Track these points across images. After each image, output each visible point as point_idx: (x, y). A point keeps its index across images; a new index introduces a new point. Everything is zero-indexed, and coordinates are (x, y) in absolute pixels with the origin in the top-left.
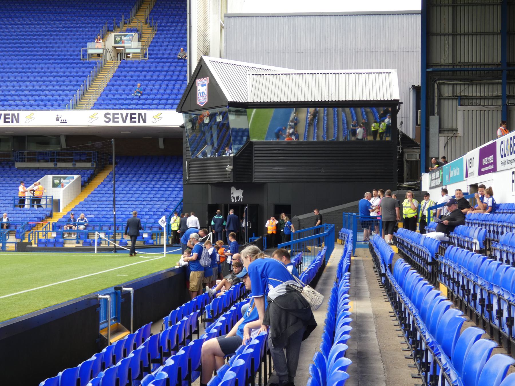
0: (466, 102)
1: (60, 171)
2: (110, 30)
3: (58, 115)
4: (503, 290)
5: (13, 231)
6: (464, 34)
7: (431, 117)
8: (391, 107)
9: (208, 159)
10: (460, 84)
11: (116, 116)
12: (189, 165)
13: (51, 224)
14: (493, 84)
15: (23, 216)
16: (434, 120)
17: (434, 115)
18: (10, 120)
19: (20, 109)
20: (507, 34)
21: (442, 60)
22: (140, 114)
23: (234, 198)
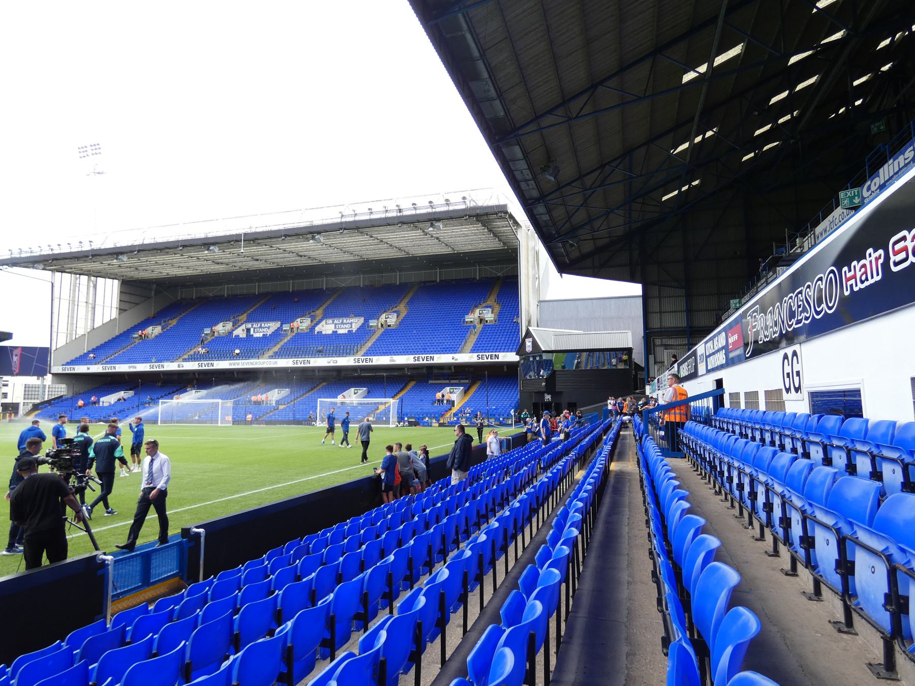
1: (452, 385)
2: (476, 307)
4: (811, 505)
8: (629, 351)
16: (651, 358)
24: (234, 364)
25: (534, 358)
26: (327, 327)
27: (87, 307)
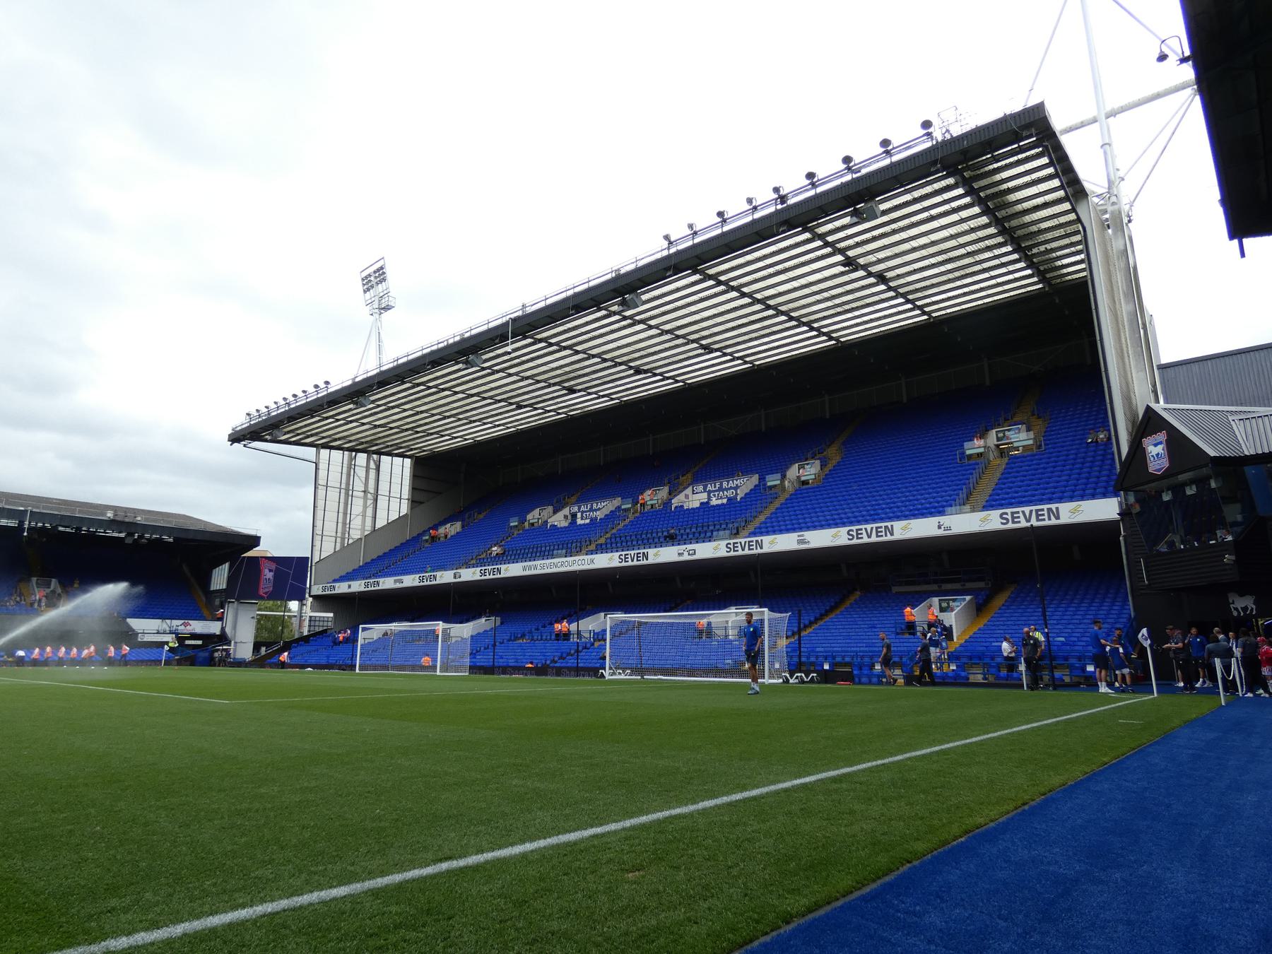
22: (1050, 510)
23: (1236, 609)
24: (530, 568)
26: (692, 498)
27: (365, 498)
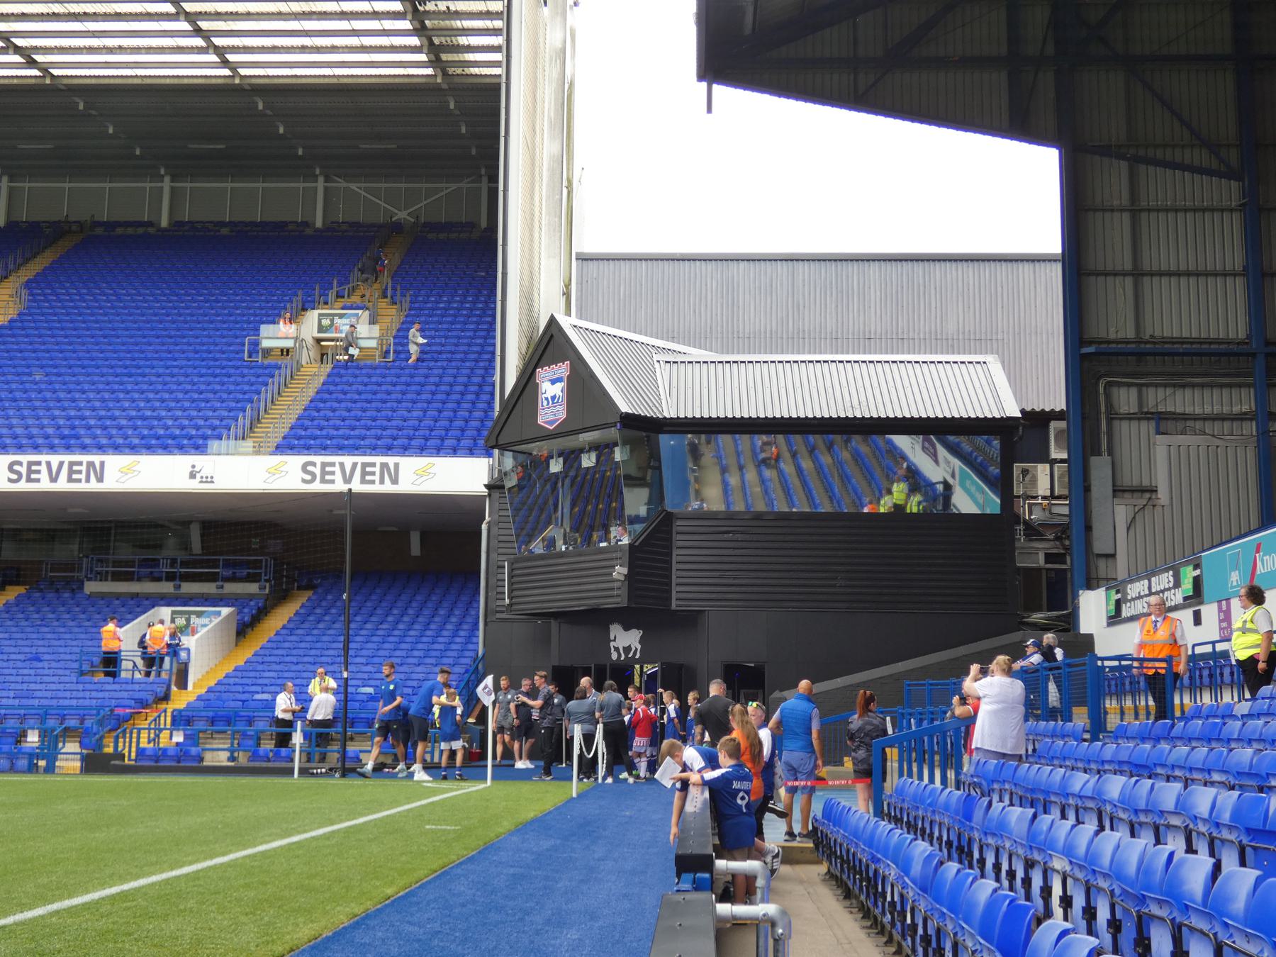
0: (1170, 425)
3: (193, 466)
5: (75, 730)
6: (1161, 274)
7: (1094, 460)
9: (561, 555)
10: (1156, 386)
11: (328, 469)
12: (511, 570)
13: (169, 714)
14: (1230, 386)
15: (100, 695)
16: (1100, 468)
17: (1100, 455)
18: (83, 477)
19: (104, 453)
20: (1258, 275)
21: (1112, 330)
23: (617, 649)
25: (571, 457)
